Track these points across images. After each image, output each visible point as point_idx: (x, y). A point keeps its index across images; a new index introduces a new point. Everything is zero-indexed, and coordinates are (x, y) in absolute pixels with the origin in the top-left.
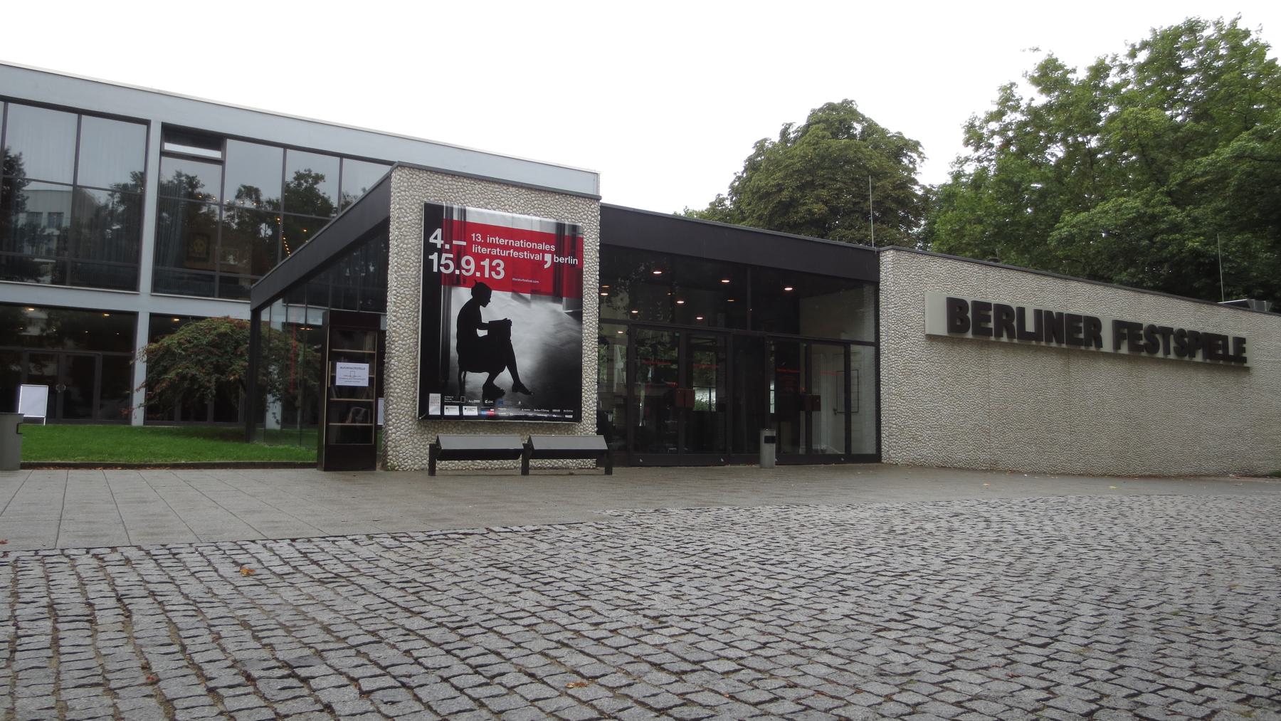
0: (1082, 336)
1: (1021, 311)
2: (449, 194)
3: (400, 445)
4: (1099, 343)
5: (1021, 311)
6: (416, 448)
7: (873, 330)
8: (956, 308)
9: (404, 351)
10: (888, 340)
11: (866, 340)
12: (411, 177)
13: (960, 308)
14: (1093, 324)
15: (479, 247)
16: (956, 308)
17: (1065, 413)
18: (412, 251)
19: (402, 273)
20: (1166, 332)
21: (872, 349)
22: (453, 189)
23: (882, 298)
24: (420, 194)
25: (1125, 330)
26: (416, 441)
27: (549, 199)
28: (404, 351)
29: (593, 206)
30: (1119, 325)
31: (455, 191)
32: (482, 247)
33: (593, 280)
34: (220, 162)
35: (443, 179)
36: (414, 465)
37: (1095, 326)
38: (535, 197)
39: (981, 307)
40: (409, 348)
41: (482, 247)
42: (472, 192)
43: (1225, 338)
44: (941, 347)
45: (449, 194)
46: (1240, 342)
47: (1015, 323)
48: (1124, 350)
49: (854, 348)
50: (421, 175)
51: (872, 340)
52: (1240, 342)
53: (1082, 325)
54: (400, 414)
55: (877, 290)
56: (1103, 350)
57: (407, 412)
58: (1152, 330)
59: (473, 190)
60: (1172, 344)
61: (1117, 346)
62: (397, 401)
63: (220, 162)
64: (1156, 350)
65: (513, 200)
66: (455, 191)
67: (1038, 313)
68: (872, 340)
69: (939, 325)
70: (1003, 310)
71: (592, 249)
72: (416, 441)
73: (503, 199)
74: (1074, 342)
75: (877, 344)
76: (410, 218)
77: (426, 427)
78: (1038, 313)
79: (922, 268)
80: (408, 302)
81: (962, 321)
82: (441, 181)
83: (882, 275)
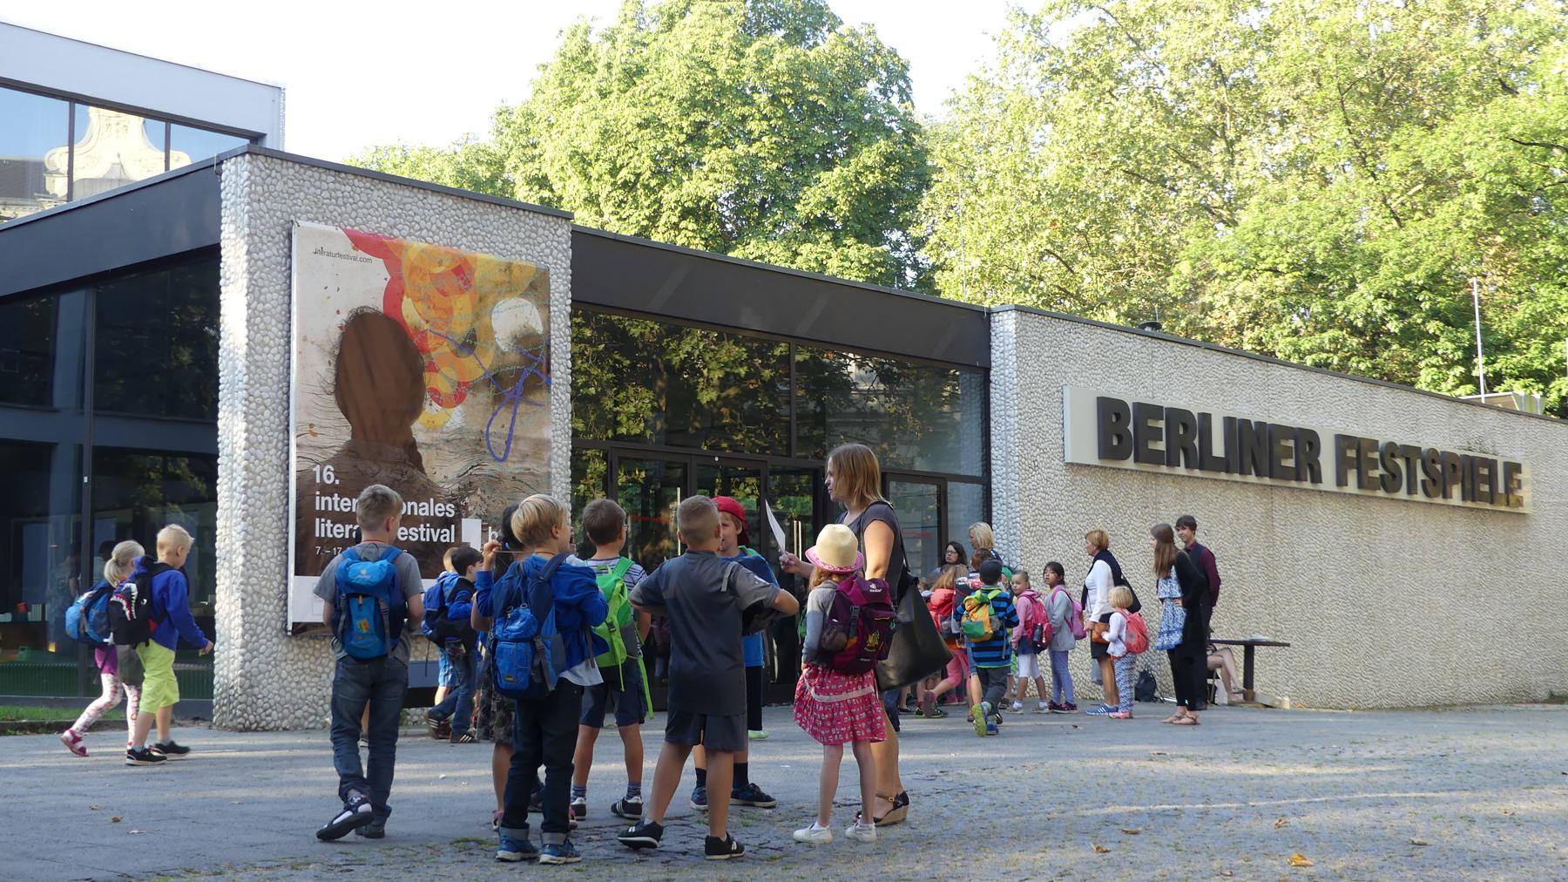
0: (1161, 446)
1: (1206, 418)
2: (331, 207)
3: (259, 683)
4: (1316, 478)
5: (1206, 418)
6: (284, 688)
7: (977, 456)
8: (1110, 413)
9: (263, 505)
10: (1007, 473)
11: (962, 472)
12: (269, 176)
13: (1118, 416)
14: (1307, 441)
15: (329, 524)
16: (1110, 413)
17: (1268, 600)
18: (272, 316)
19: (257, 357)
20: (1409, 453)
21: (977, 489)
22: (337, 198)
23: (995, 397)
24: (284, 207)
25: (1354, 452)
26: (284, 674)
27: (491, 217)
28: (263, 505)
29: (559, 232)
30: (1343, 442)
31: (340, 202)
32: (334, 523)
33: (562, 368)
34: (1249, 647)
35: (320, 180)
36: (283, 719)
37: (1311, 444)
38: (469, 214)
39: (1147, 411)
40: (271, 499)
41: (334, 523)
42: (368, 205)
43: (1491, 465)
44: (1088, 483)
45: (331, 207)
46: (1513, 468)
47: (1196, 442)
48: (1352, 487)
49: (950, 485)
50: (284, 171)
51: (976, 471)
52: (1513, 468)
53: (1162, 424)
54: (257, 624)
55: (986, 382)
56: (1321, 487)
57: (269, 620)
58: (1392, 450)
59: (369, 200)
60: (1420, 476)
61: (1341, 481)
62: (253, 602)
63: (1249, 647)
64: (1397, 489)
65: (433, 219)
66: (340, 202)
67: (1229, 421)
68: (976, 471)
69: (1083, 442)
70: (1179, 418)
71: (560, 312)
72: (284, 674)
73: (417, 218)
74: (1274, 471)
75: (985, 480)
76: (268, 253)
77: (300, 647)
78: (1229, 421)
79: (1060, 345)
80: (267, 413)
81: (1120, 438)
82: (318, 184)
83: (996, 355)
